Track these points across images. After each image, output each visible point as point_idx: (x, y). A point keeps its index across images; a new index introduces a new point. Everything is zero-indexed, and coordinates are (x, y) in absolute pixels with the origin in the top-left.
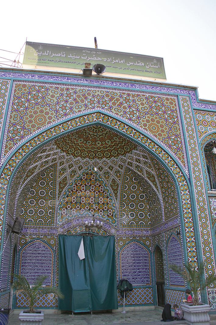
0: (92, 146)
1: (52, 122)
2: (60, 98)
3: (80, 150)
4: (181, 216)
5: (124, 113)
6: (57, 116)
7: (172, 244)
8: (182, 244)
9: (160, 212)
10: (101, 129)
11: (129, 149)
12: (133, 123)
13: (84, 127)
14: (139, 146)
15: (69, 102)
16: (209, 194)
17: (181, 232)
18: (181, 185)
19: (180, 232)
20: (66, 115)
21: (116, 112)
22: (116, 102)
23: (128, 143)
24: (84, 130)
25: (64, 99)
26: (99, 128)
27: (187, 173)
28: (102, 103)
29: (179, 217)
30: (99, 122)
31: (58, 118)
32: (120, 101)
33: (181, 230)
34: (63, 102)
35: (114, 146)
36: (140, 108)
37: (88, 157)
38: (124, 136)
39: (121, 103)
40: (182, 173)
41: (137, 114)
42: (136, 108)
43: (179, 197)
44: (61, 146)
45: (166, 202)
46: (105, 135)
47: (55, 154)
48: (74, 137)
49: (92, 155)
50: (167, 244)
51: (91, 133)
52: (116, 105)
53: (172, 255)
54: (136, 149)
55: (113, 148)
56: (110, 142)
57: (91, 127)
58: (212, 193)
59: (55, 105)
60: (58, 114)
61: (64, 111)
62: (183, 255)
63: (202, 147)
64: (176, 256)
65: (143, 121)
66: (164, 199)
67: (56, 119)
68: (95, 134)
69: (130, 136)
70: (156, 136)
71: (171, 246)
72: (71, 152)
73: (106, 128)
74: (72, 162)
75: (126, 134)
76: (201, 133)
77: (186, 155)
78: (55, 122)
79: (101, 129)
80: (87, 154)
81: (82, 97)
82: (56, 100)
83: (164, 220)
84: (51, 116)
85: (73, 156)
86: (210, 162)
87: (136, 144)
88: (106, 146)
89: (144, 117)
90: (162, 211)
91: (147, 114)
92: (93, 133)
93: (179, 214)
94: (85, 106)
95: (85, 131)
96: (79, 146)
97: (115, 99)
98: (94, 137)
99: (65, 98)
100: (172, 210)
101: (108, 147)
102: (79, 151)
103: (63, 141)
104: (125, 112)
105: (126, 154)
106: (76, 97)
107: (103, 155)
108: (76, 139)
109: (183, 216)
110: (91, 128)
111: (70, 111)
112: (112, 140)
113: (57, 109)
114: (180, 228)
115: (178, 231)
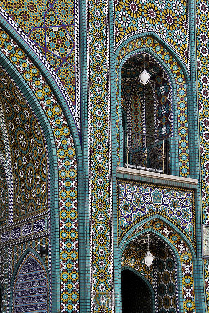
4: (53, 215)
7: (26, 274)
8: (50, 275)
9: (4, 202)
16: (120, 172)
17: (50, 249)
18: (60, 144)
19: (47, 248)
20: (45, 50)
27: (77, 119)
29: (49, 217)
33: (50, 245)
40: (66, 118)
43: (52, 172)
45: (19, 180)
50: (15, 271)
53: (25, 297)
58: (125, 173)
61: (53, 45)
62: (51, 297)
63: (119, 65)
64: (33, 299)
66: (16, 173)
70: (13, 17)
71: (25, 277)
76: (120, 31)
77: (79, 77)
83: (12, 221)
86: (129, 103)
90: (10, 200)
93: (49, 209)
100: (33, 200)
109: (57, 216)
114: (50, 241)
115: (44, 246)
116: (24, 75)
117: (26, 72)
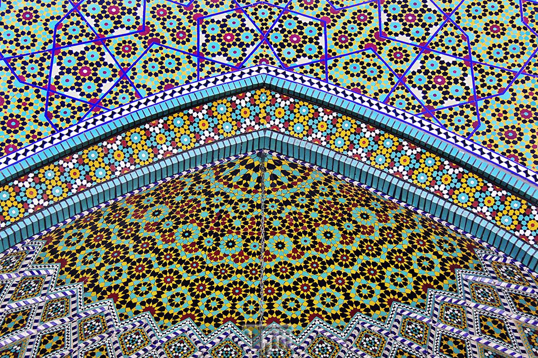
0: (247, 263)
1: (26, 142)
2: (66, 22)
3: (186, 283)
5: (395, 79)
6: (48, 116)
10: (285, 173)
11: (437, 266)
12: (445, 126)
13: (194, 161)
14: (485, 244)
15: (113, 45)
20: (95, 105)
21: (355, 80)
22: (352, 28)
23: (427, 234)
24: (197, 178)
25: (88, 30)
26: (271, 167)
28: (281, 38)
30: (268, 133)
31: (55, 121)
32: (375, 24)
34: (80, 43)
35: (358, 253)
36: (480, 49)
37: (232, 319)
38: (400, 201)
39: (381, 36)
41: (468, 81)
42: (459, 50)
44: (86, 268)
46: (307, 201)
47: (56, 309)
48: (148, 218)
49: (251, 307)
51: (236, 194)
52: (355, 47)
54: (471, 263)
55: (357, 265)
56: (337, 234)
57: (231, 165)
59: (43, 59)
60: (57, 102)
61: (89, 87)
65: (500, 115)
67: (46, 131)
68: (258, 199)
69: (430, 197)
72: (145, 298)
73: (307, 165)
74: (149, 348)
75: (412, 189)
78: (39, 144)
79: (285, 173)
80: (227, 305)
81: (180, 15)
82: (43, 37)
84: (16, 112)
85: (157, 319)
87: (469, 236)
88: (318, 255)
89: (507, 96)
91: (522, 77)
92: (244, 195)
94: (194, 59)
95: (203, 186)
96: (181, 262)
97: (348, 15)
98: (251, 215)
99: (92, 22)
101: (330, 262)
102: (182, 289)
103: (93, 242)
104: (402, 80)
105: (424, 297)
106: (149, 17)
107: (310, 303)
108: (164, 227)
110: (233, 169)
111: (117, 85)
112: (345, 225)
113: (49, 77)
116: (52, 199)
117: (91, 174)
